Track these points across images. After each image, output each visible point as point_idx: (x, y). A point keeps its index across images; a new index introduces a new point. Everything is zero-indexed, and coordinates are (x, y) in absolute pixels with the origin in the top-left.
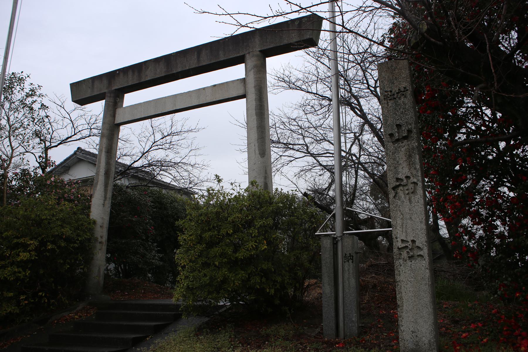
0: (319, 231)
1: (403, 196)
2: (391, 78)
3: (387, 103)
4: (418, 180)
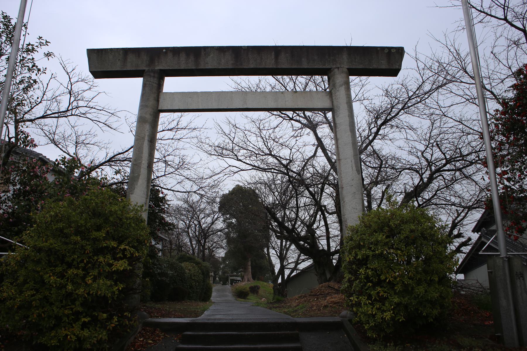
0: (481, 251)
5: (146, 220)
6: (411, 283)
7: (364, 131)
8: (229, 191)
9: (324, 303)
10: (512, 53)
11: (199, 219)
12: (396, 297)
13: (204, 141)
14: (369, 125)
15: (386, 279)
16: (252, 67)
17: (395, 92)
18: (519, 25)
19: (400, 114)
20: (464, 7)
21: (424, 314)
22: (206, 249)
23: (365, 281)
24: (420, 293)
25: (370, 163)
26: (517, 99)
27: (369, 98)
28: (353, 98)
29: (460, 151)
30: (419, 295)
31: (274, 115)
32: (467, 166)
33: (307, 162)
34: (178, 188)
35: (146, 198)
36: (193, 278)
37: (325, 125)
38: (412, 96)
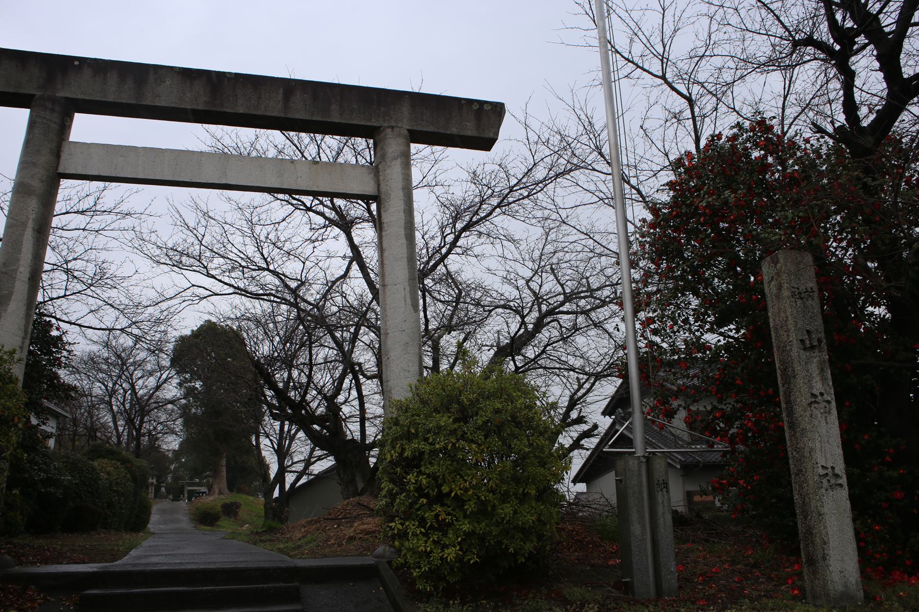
0: (607, 447)
3: (796, 302)
5: (21, 378)
6: (492, 499)
7: (433, 238)
8: (193, 331)
9: (350, 532)
10: (670, 132)
11: (132, 380)
12: (466, 522)
13: (147, 238)
14: (442, 228)
15: (451, 491)
16: (241, 111)
17: (488, 177)
18: (682, 89)
19: (494, 214)
20: (603, 50)
21: (511, 550)
22: (144, 435)
23: (416, 495)
24: (506, 515)
25: (439, 294)
26: (674, 204)
27: (445, 184)
28: (414, 184)
29: (588, 282)
30: (503, 519)
31: (278, 199)
32: (598, 307)
33: (332, 286)
34: (90, 320)
35: (24, 338)
36: (115, 488)
37: (365, 224)
38: (515, 185)
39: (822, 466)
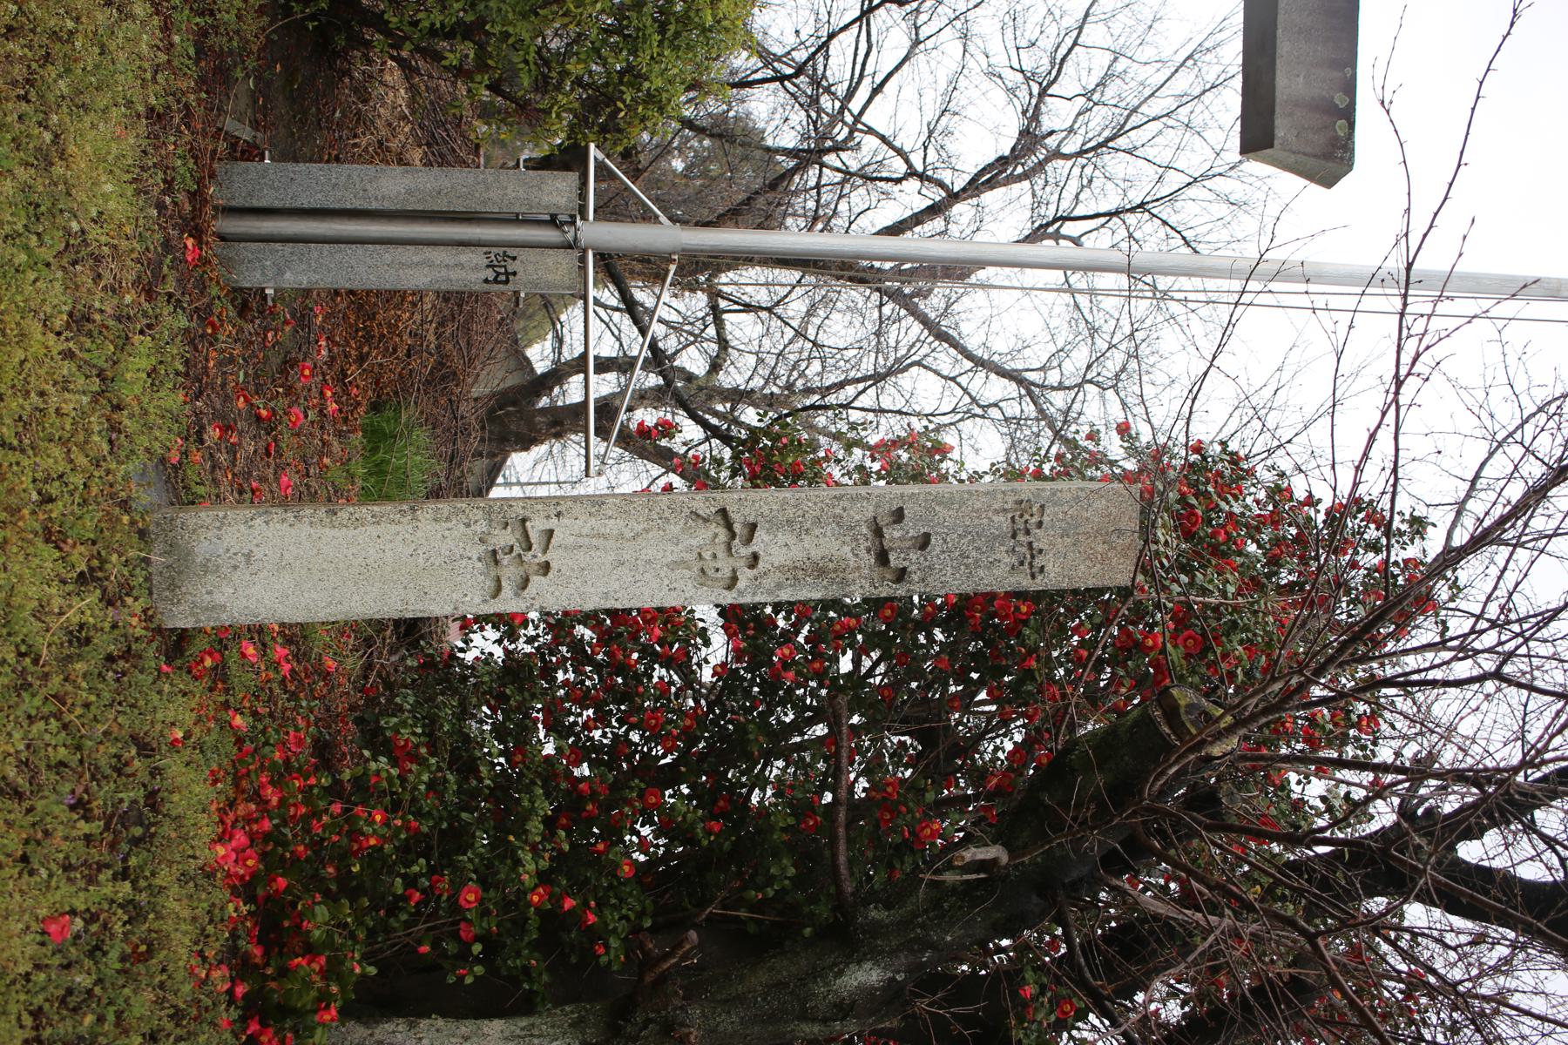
0: (601, 156)
1: (694, 542)
2: (1081, 530)
4: (741, 593)
39: (550, 533)
